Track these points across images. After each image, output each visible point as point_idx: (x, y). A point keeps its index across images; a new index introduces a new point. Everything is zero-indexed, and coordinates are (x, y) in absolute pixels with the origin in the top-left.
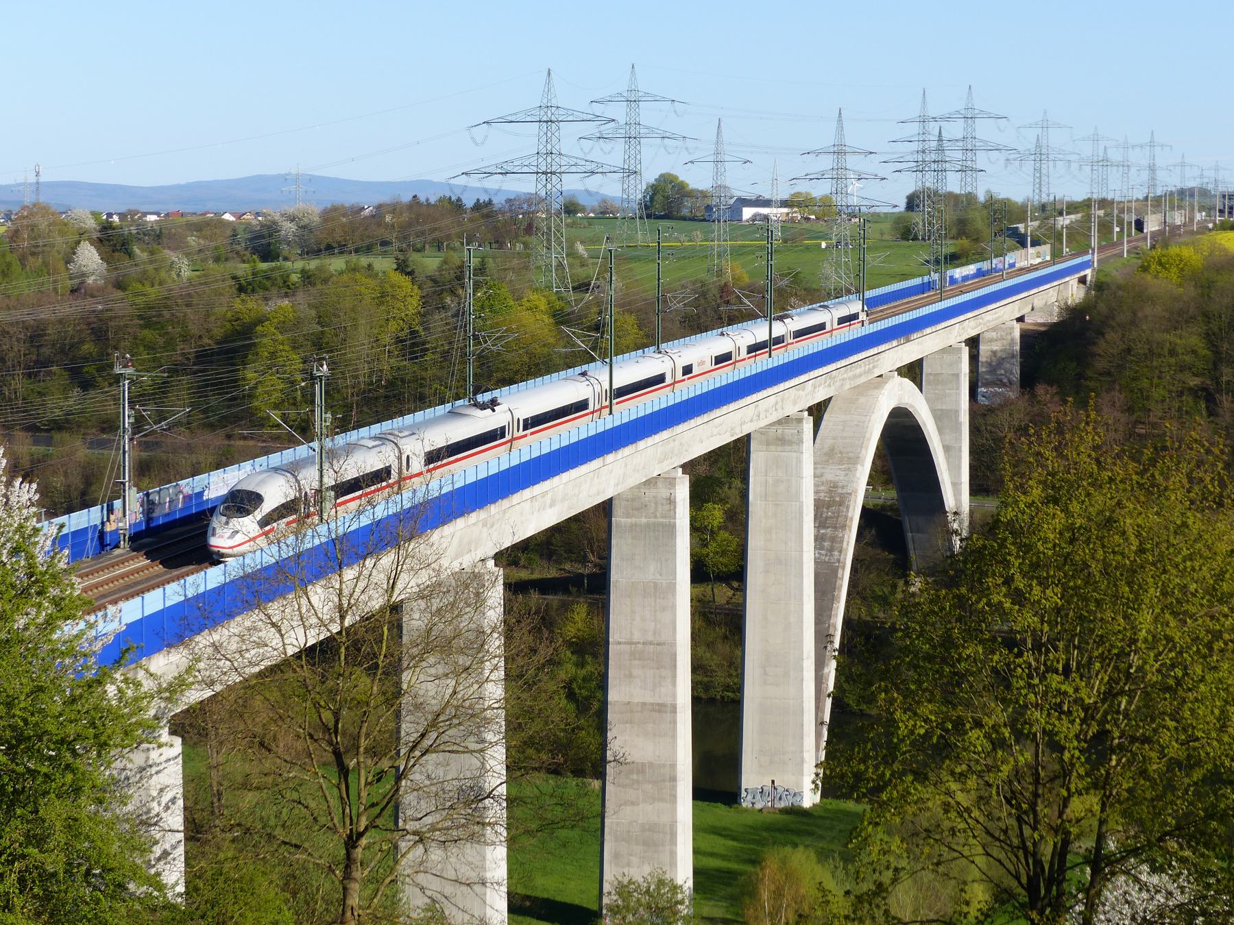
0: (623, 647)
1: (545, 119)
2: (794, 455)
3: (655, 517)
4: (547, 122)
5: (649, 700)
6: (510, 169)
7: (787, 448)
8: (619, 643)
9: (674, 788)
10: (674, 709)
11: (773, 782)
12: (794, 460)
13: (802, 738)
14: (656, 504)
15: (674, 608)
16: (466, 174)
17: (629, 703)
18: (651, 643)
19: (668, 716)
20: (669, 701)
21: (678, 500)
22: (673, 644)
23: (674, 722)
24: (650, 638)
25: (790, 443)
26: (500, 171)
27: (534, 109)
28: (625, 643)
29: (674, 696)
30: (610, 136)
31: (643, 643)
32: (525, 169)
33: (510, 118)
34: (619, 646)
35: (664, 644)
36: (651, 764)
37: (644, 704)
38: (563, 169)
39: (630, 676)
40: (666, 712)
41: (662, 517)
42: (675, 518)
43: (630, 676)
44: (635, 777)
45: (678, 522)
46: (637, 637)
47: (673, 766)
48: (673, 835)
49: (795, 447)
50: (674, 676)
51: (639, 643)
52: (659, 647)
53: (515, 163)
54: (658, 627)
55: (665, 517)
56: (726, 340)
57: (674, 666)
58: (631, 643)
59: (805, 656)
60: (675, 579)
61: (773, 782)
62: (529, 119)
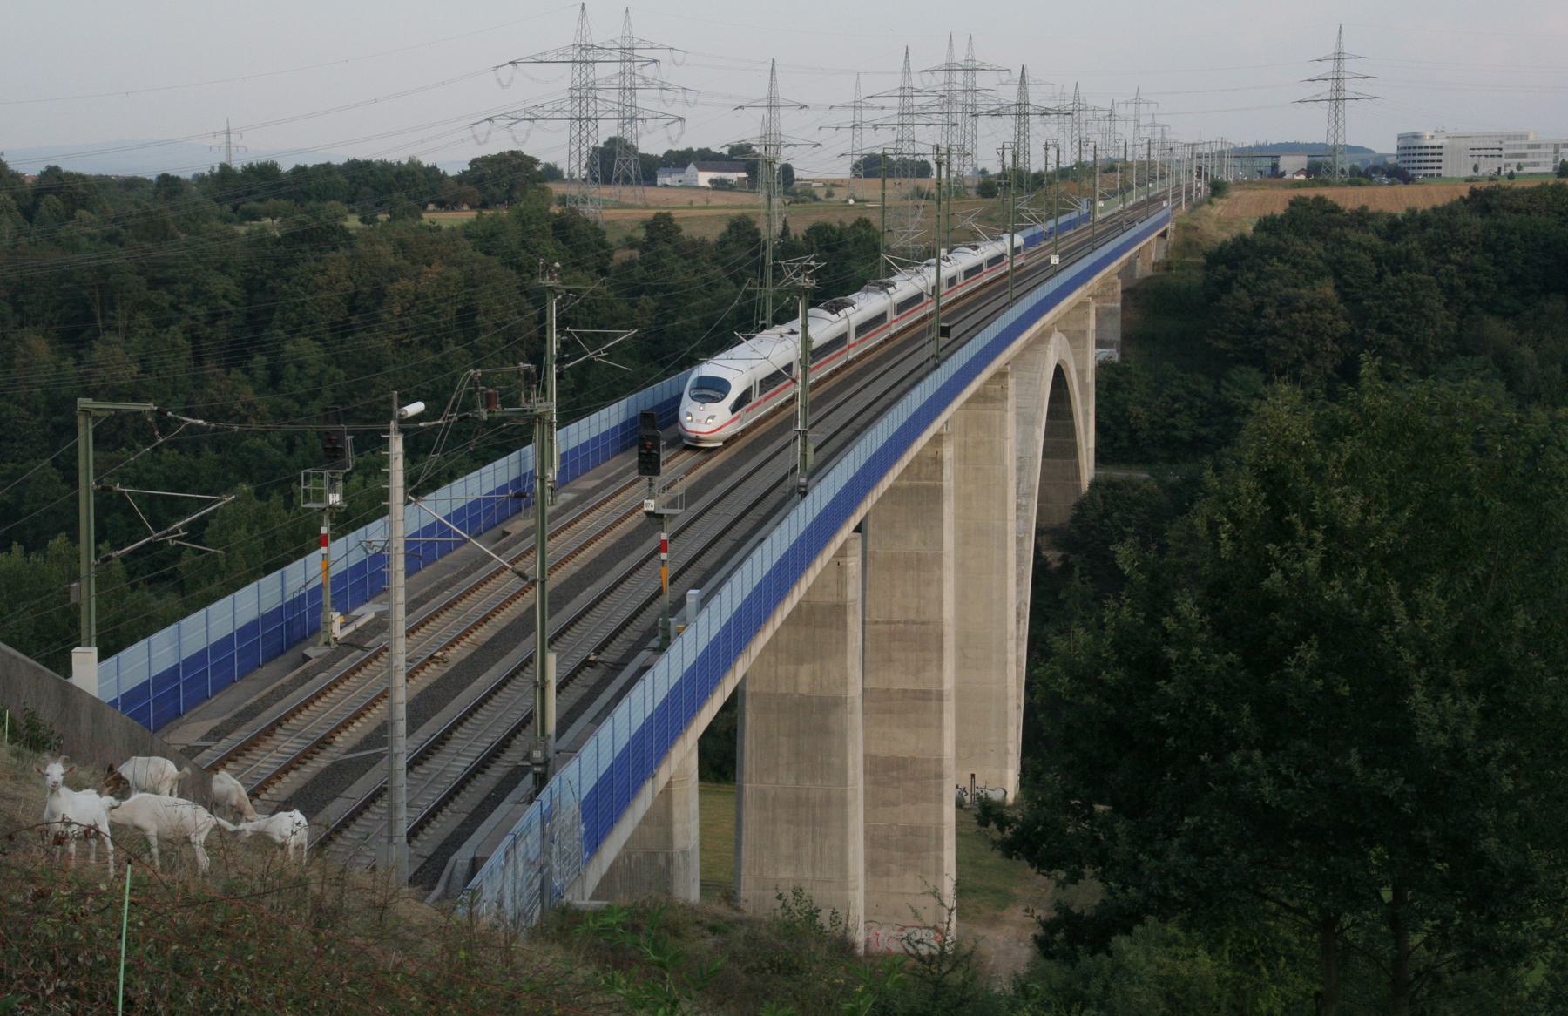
0: (881, 627)
1: (578, 59)
2: (997, 412)
3: (919, 479)
4: (581, 62)
5: (911, 686)
6: (540, 114)
7: (990, 405)
8: (877, 622)
9: (940, 786)
10: (940, 697)
11: (973, 776)
12: (998, 420)
13: (1006, 727)
14: (920, 463)
15: (940, 581)
16: (489, 119)
17: (888, 690)
18: (914, 622)
19: (933, 704)
20: (934, 687)
21: (944, 460)
22: (939, 623)
23: (941, 712)
24: (912, 616)
25: (993, 400)
26: (528, 116)
27: (567, 47)
28: (883, 622)
29: (940, 682)
30: (604, 86)
31: (905, 622)
32: (558, 115)
33: (539, 58)
34: (876, 627)
35: (929, 623)
36: (914, 759)
37: (905, 691)
38: (599, 115)
39: (890, 660)
40: (930, 700)
41: (926, 479)
42: (942, 480)
43: (890, 660)
44: (895, 774)
45: (945, 484)
46: (896, 617)
47: (940, 761)
48: (939, 839)
49: (999, 405)
50: (941, 660)
51: (899, 622)
52: (922, 627)
53: (546, 108)
54: (922, 602)
55: (931, 479)
56: (916, 280)
57: (940, 649)
58: (889, 622)
59: (1009, 636)
60: (942, 549)
61: (973, 776)
62: (560, 59)
